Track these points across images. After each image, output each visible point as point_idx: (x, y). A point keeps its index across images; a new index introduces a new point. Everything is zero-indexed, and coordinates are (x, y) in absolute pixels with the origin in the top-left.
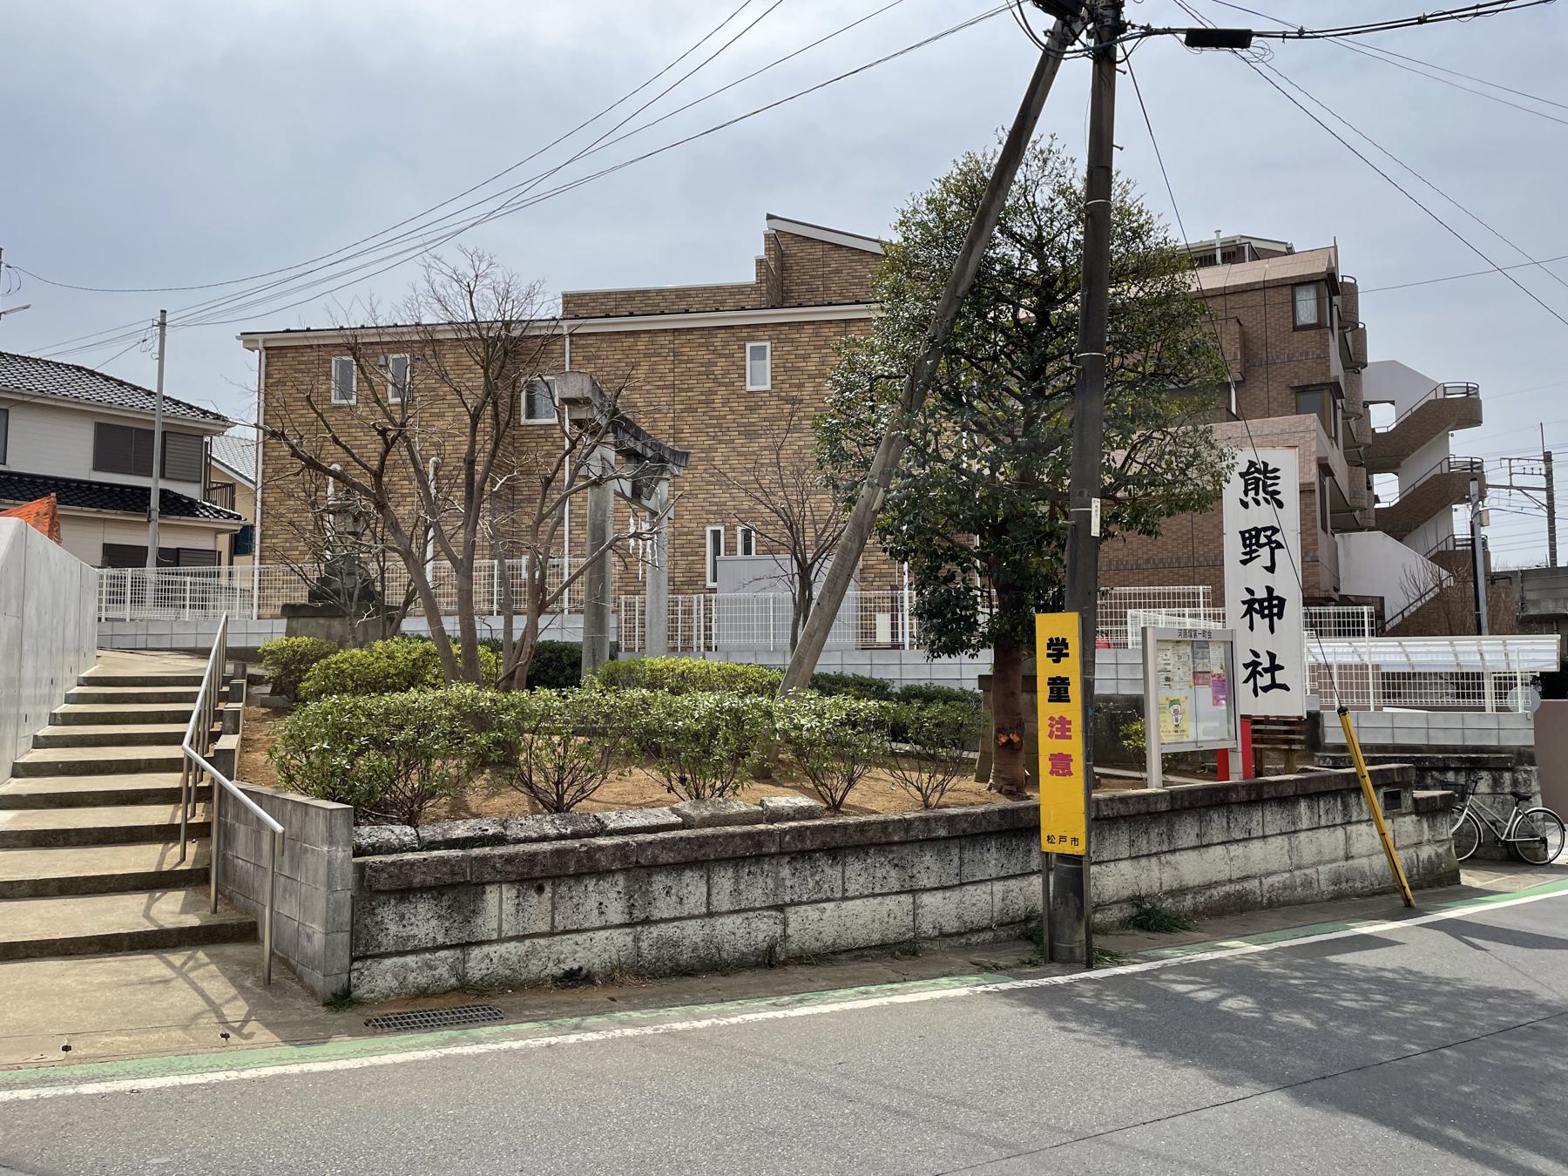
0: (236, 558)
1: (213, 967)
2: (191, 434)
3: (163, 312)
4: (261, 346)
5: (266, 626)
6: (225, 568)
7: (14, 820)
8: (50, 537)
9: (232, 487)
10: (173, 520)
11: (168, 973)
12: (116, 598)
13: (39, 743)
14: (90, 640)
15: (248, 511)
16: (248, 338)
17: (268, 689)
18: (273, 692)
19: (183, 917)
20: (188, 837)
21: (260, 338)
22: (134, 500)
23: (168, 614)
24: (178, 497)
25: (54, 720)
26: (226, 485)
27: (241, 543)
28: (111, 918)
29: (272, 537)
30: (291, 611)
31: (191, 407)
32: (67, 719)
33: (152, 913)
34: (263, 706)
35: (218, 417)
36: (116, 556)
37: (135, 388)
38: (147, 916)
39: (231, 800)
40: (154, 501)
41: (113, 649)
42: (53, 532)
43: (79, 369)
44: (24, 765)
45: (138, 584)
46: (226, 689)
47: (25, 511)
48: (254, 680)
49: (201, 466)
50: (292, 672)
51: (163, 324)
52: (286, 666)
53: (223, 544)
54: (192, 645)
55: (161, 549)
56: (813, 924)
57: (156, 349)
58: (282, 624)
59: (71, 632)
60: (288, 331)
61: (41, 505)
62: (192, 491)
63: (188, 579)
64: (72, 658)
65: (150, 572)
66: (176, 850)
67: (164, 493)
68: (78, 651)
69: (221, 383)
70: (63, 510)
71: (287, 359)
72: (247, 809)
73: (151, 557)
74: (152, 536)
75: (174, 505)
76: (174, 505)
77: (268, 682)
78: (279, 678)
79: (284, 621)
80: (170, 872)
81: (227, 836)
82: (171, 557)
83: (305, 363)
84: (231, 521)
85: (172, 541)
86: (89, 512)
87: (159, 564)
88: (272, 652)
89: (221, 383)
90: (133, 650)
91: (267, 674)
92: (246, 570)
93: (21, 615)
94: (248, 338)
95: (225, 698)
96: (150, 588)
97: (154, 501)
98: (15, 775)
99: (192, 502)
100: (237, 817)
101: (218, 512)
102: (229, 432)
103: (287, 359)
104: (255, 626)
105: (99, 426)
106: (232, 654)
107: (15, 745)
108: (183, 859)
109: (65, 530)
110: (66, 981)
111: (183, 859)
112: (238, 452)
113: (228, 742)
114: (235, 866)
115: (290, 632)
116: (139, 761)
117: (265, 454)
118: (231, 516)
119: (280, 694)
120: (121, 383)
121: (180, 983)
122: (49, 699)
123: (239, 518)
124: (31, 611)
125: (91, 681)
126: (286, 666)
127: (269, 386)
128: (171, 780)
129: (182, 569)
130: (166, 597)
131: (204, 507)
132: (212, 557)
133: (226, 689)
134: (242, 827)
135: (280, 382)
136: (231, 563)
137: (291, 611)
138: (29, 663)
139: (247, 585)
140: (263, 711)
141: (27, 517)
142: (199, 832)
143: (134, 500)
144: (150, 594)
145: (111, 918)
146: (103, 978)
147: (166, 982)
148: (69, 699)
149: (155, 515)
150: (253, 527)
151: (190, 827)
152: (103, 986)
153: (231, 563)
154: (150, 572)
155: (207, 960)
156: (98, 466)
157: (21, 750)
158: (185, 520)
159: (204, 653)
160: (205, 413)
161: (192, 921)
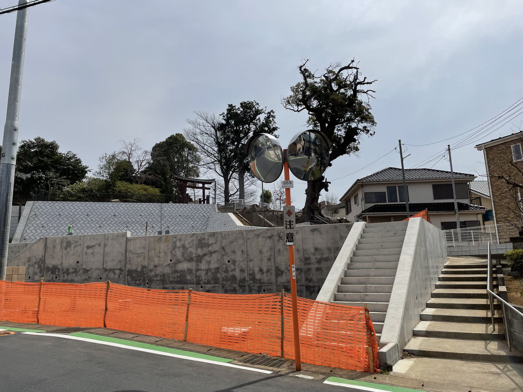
0: (485, 223)
1: (515, 372)
2: (464, 181)
3: (449, 146)
4: (483, 148)
5: (503, 246)
6: (482, 227)
7: (435, 311)
8: (427, 220)
9: (479, 198)
10: (462, 212)
11: (498, 371)
12: (449, 239)
13: (437, 287)
14: (445, 254)
15: (488, 206)
16: (479, 147)
17: (510, 269)
18: (512, 270)
19: (499, 351)
20: (495, 323)
21: (483, 145)
22: (449, 207)
23: (465, 244)
24: (462, 204)
25: (440, 279)
26: (477, 198)
27: (487, 216)
28: (474, 348)
29: (500, 213)
30: (513, 240)
31: (461, 174)
32: (444, 279)
33: (488, 348)
34: (509, 275)
35: (470, 175)
36: (446, 226)
37: (442, 172)
38: (486, 348)
39: (509, 310)
40: (456, 207)
41: (452, 256)
42: (428, 220)
43: (425, 169)
44: (435, 294)
45: (456, 234)
46: (494, 269)
47: (419, 215)
48: (504, 266)
49: (467, 192)
50: (519, 262)
51: (449, 150)
52: (515, 260)
53: (480, 218)
54: (477, 254)
55: (461, 222)
56: (121, 336)
57: (449, 158)
58: (511, 245)
59: (439, 251)
60: (492, 140)
61: (423, 212)
62: (466, 201)
63: (472, 231)
64: (441, 259)
65: (459, 230)
66: (491, 326)
67: (458, 203)
68: (442, 257)
69: (473, 164)
70: (430, 213)
71: (494, 151)
72: (516, 313)
73: (458, 225)
74: (457, 218)
75: (463, 207)
76: (463, 207)
77: (508, 267)
78: (514, 265)
79: (512, 244)
80: (491, 334)
81: (510, 323)
82: (464, 224)
83: (501, 150)
84: (481, 210)
85: (463, 219)
86: (435, 213)
87: (461, 227)
88: (508, 256)
89: (473, 164)
90: (458, 256)
91: (509, 264)
92: (491, 227)
93: (426, 246)
94: (479, 147)
95: (496, 272)
96: (459, 235)
97: (456, 207)
98: (432, 297)
99: (467, 205)
100: (513, 317)
101: (476, 207)
102: (475, 179)
103: (494, 151)
104: (499, 246)
105: (434, 187)
106: (493, 257)
107: (431, 288)
108: (494, 330)
109: (431, 219)
110: (464, 368)
111: (494, 330)
112: (481, 185)
113: (503, 289)
114: (515, 335)
115: (515, 248)
116: (470, 294)
117: (491, 185)
118: (481, 208)
119: (515, 271)
120: (438, 171)
121: (503, 375)
122: (437, 273)
123: (484, 208)
124: (428, 245)
125: (448, 267)
126: (515, 260)
127: (490, 161)
128: (482, 301)
129: (467, 228)
130: (466, 238)
131: (471, 206)
132: (476, 223)
133: (494, 269)
134: (515, 321)
135: (493, 159)
136: (484, 225)
137: (513, 240)
138: (430, 261)
139: (494, 232)
140: (509, 277)
141: (420, 216)
142: (499, 321)
143: (449, 207)
144: (460, 238)
145: (474, 348)
146: (476, 369)
147: (499, 374)
148: (443, 273)
149: (457, 211)
150: (491, 211)
151: (495, 319)
152: (476, 372)
153: (484, 225)
154: (459, 230)
155: (511, 369)
156: (435, 198)
157: (432, 289)
158: (466, 212)
159: (485, 257)
160: (466, 175)
161: (503, 353)
